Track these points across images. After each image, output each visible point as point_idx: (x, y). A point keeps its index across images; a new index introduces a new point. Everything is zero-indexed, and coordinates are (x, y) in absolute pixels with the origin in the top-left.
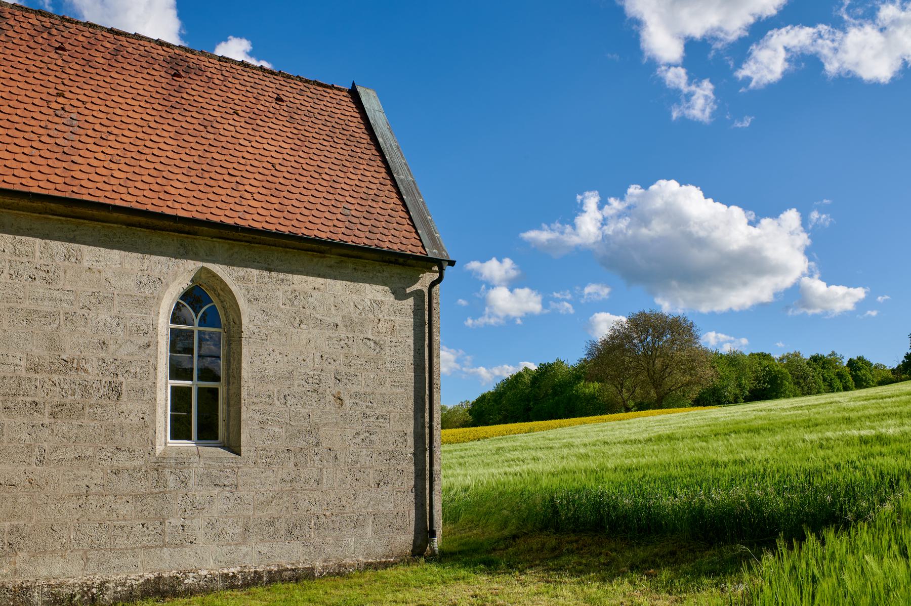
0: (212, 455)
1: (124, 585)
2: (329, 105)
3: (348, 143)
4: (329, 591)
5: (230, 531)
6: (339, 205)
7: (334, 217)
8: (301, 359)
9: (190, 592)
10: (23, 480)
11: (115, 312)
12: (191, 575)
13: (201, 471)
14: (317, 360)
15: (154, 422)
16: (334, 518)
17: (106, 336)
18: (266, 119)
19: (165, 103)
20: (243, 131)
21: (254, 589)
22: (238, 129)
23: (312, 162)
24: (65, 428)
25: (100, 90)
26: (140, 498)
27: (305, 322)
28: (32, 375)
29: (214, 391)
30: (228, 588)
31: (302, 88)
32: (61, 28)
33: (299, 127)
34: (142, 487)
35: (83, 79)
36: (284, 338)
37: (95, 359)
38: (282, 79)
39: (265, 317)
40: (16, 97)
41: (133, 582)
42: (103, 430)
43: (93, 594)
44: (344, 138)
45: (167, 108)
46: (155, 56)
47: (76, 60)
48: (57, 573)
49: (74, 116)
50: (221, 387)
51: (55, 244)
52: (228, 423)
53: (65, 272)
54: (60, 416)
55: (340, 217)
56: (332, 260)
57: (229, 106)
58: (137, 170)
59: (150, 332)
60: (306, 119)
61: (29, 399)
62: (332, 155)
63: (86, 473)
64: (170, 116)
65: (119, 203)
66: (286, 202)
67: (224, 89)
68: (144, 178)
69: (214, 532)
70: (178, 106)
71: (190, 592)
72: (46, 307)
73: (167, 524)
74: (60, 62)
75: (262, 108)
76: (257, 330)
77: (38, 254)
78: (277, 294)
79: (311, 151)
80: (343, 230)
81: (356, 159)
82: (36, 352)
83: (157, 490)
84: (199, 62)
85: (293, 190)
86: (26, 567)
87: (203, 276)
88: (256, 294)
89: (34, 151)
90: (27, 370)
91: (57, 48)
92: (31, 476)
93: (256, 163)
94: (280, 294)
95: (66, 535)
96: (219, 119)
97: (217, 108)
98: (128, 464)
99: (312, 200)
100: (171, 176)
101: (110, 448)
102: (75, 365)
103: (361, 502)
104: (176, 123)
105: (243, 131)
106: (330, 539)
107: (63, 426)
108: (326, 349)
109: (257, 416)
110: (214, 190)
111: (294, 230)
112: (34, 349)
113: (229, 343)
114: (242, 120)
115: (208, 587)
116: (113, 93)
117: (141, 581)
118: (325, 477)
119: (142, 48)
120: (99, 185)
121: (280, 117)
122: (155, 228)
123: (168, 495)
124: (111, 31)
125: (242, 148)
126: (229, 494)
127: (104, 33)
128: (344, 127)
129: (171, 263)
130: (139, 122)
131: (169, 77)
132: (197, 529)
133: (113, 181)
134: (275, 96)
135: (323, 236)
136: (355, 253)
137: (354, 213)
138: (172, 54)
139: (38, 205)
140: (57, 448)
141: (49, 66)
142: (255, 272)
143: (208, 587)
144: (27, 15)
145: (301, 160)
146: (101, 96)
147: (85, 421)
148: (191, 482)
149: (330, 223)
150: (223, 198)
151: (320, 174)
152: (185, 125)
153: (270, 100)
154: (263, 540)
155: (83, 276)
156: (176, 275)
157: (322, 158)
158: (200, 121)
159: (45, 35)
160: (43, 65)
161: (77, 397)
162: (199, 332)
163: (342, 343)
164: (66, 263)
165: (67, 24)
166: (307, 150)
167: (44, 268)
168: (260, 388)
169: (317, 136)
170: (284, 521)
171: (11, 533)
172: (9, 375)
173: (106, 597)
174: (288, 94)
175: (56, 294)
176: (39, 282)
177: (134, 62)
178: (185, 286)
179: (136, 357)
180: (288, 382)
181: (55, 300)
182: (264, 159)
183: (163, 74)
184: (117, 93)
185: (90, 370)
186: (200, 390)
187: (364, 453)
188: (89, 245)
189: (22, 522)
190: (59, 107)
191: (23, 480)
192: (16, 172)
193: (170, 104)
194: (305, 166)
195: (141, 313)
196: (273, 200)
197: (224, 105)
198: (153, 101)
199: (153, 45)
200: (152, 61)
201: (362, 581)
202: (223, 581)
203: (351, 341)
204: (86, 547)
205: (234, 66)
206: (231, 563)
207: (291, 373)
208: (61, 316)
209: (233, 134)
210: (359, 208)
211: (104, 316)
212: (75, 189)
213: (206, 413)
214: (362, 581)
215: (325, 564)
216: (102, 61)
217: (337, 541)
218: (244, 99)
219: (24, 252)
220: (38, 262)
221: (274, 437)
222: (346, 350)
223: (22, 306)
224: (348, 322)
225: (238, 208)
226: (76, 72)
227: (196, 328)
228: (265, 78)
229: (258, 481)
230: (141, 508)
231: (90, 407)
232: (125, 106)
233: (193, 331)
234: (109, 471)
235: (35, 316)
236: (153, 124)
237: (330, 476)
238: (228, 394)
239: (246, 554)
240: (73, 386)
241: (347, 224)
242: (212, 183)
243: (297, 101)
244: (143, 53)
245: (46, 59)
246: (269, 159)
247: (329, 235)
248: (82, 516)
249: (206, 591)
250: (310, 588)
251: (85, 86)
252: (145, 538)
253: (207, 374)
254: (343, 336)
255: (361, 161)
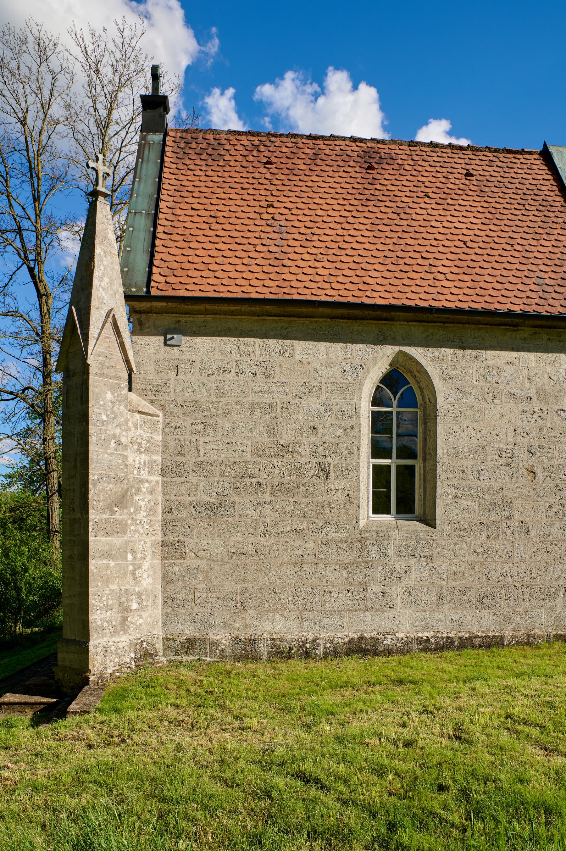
0: (409, 528)
1: (332, 642)
2: (520, 171)
3: (541, 208)
4: (517, 659)
5: (425, 599)
6: (531, 274)
7: (527, 288)
8: (494, 434)
9: (389, 652)
10: (250, 549)
11: (323, 399)
12: (389, 637)
13: (399, 543)
14: (511, 435)
15: (358, 498)
16: (524, 589)
17: (316, 422)
18: (456, 197)
19: (361, 197)
20: (434, 213)
21: (445, 653)
22: (430, 211)
23: (503, 234)
24: (283, 505)
25: (304, 195)
26: (345, 566)
27: (498, 397)
28: (256, 459)
29: (411, 469)
30: (422, 651)
31: (491, 158)
32: (268, 143)
33: (490, 200)
34: (349, 556)
35: (288, 188)
36: (478, 414)
37: (307, 443)
38: (471, 153)
39: (460, 395)
40: (234, 214)
41: (340, 640)
42: (314, 506)
43: (307, 648)
44: (536, 203)
45: (362, 202)
46: (349, 153)
47: (282, 171)
48: (278, 628)
49: (282, 223)
50: (418, 464)
51: (271, 342)
52: (425, 498)
53: (280, 366)
54: (279, 494)
55: (533, 287)
56: (525, 332)
57: (419, 189)
58: (338, 265)
59: (353, 416)
60: (496, 190)
61: (254, 480)
62: (524, 224)
63: (301, 544)
64: (366, 209)
65: (324, 298)
66: (478, 278)
67: (415, 173)
68: (345, 272)
69: (411, 599)
70: (372, 198)
71: (389, 652)
72: (266, 399)
73: (369, 590)
74: (268, 176)
75: (452, 186)
76: (451, 408)
77: (258, 352)
78: (471, 371)
79: (502, 223)
80: (537, 301)
81: (550, 225)
82: (259, 439)
83: (360, 560)
84: (390, 151)
85: (485, 265)
86: (254, 622)
87: (400, 360)
88: (450, 373)
89: (251, 260)
90: (252, 455)
91: (265, 163)
92: (257, 546)
93: (448, 243)
94: (473, 371)
95: (285, 597)
96: (411, 205)
97: (408, 194)
98: (336, 536)
99: (505, 273)
100: (368, 267)
101: (320, 522)
102: (290, 449)
103: (552, 574)
104: (371, 215)
105: (434, 213)
106: (520, 610)
107: (281, 503)
108: (519, 422)
109: (451, 491)
110: (409, 275)
111: (487, 306)
112: (257, 436)
113: (425, 422)
114: (433, 201)
115: (404, 649)
116: (315, 195)
117: (347, 640)
118: (516, 550)
119: (337, 148)
120: (306, 284)
121: (470, 193)
122: (355, 318)
123: (369, 565)
124: (310, 137)
125: (434, 230)
126: (424, 564)
127: (304, 141)
128: (536, 192)
129: (371, 350)
130: (338, 219)
131: (364, 171)
132: (395, 595)
133: (318, 278)
134: (465, 172)
135: (516, 308)
136: (549, 323)
137: (548, 281)
138: (365, 149)
139: (256, 309)
140: (277, 523)
141: (260, 181)
142: (449, 351)
143: (404, 649)
144: (239, 137)
145: (492, 234)
146: (304, 200)
147: (300, 499)
148: (390, 553)
149: (523, 295)
150: (418, 282)
151: (512, 245)
152: (379, 215)
153: (459, 176)
154: (455, 608)
155: (295, 368)
156: (375, 360)
157: (514, 229)
158: (393, 210)
159: (255, 153)
160: (254, 181)
161: (293, 477)
162: (398, 413)
163: (536, 416)
164: (281, 358)
165: (273, 139)
166: (498, 222)
167: (263, 364)
168: (454, 464)
169: (508, 206)
170: (475, 590)
171: (242, 594)
172: (238, 460)
173: (317, 652)
174: (477, 168)
175: (274, 387)
176: (259, 377)
177: (332, 163)
178: (384, 371)
179: (342, 440)
180: (482, 457)
181: (273, 392)
182: (456, 238)
183: (357, 169)
184: (318, 195)
185: (303, 453)
186: (398, 467)
187: (557, 525)
188: (300, 340)
189: (250, 585)
190: (269, 217)
191: (250, 549)
192: (238, 282)
193: (365, 197)
194: (496, 240)
195: (345, 398)
196: (465, 278)
197: (415, 189)
198: (349, 197)
199: (347, 143)
200: (347, 159)
201: (551, 652)
202: (418, 644)
203: (545, 414)
204: (301, 609)
205: (423, 149)
206: (425, 628)
207: (484, 448)
208: (278, 406)
209: (425, 217)
210: (553, 275)
211: (314, 403)
212: (286, 290)
213: (404, 490)
214: (551, 652)
215: (514, 634)
216: (303, 167)
217: (527, 611)
218: (434, 180)
219: (247, 352)
220: (258, 359)
221: (467, 510)
222: (540, 423)
223: (246, 400)
224: (542, 394)
225: (431, 290)
226: (282, 182)
227: (394, 409)
228: (454, 155)
229: (451, 552)
230: (346, 575)
231: (304, 486)
232: (325, 207)
233: (391, 413)
234: (320, 543)
235: (257, 408)
236: (351, 220)
237: (522, 548)
238: (424, 470)
239: (439, 620)
240: (289, 467)
241: (541, 294)
242: (406, 268)
243: (486, 174)
244: (339, 152)
245: (257, 175)
246: (461, 237)
247: (522, 307)
248: (298, 581)
249: (403, 652)
250: (499, 656)
251: (291, 194)
252: (350, 602)
253: (406, 452)
254: (537, 409)
255: (555, 226)
